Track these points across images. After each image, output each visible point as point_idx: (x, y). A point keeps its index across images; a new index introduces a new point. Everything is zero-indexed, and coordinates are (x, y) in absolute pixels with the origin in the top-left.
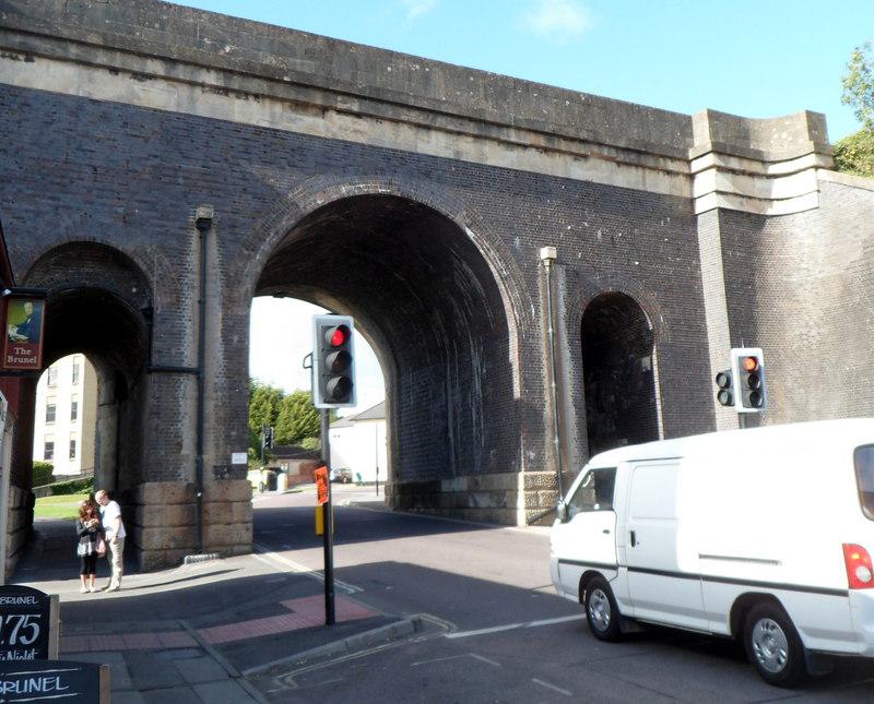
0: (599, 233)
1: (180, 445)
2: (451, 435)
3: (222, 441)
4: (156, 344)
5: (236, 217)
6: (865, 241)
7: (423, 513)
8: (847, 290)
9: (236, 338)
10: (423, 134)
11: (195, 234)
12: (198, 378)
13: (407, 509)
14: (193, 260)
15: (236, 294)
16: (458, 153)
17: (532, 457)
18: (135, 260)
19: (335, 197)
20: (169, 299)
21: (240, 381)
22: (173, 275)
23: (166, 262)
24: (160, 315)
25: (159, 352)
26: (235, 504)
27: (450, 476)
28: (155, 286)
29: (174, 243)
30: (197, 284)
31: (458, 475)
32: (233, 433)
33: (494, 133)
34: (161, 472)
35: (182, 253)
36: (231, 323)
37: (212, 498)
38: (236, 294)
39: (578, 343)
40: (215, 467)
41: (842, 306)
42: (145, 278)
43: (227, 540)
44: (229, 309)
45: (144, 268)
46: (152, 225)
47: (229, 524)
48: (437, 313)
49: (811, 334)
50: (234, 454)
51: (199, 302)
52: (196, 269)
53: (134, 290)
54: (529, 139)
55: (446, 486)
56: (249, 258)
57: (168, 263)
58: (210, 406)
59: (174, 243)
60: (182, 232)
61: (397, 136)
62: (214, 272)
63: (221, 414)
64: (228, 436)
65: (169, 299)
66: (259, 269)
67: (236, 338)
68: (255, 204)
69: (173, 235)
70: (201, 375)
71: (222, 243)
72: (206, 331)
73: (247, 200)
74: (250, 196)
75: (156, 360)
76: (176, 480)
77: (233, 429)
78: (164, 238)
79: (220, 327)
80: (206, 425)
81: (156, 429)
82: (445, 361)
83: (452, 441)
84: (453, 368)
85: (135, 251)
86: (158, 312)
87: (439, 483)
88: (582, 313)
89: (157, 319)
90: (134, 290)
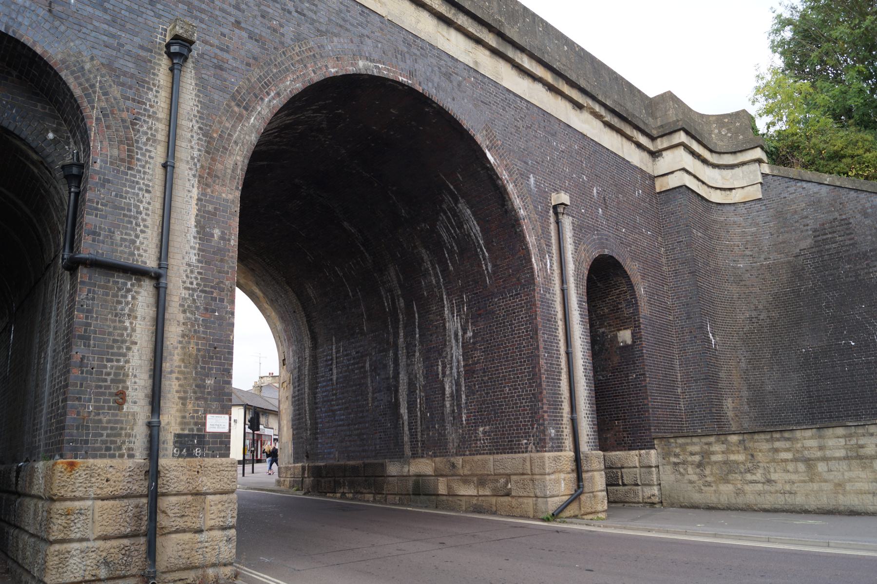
0: (595, 191)
1: (121, 397)
2: (404, 411)
3: (190, 394)
4: (89, 220)
5: (225, 55)
6: (815, 231)
7: (352, 499)
8: (797, 273)
9: (217, 232)
10: (443, 29)
11: (164, 63)
12: (157, 288)
13: (323, 493)
14: (160, 101)
15: (219, 166)
16: (476, 63)
17: (553, 435)
18: (63, 74)
19: (351, 70)
20: (115, 152)
21: (222, 300)
22: (125, 115)
23: (116, 91)
24: (97, 173)
25: (94, 233)
26: (210, 497)
27: (398, 455)
28: (93, 126)
29: (131, 67)
30: (161, 136)
31: (415, 456)
32: (208, 382)
33: (510, 53)
34: (86, 442)
35: (143, 83)
36: (210, 208)
37: (172, 488)
38: (219, 166)
39: (585, 305)
40: (178, 436)
41: (793, 291)
42: (76, 108)
43: (198, 559)
44: (208, 185)
45: (77, 92)
46: (96, 29)
47: (200, 531)
48: (392, 273)
49: (761, 317)
50: (209, 416)
51: (165, 166)
52: (162, 115)
53: (51, 136)
54: (539, 71)
55: (393, 469)
56: (240, 118)
57: (119, 96)
58: (173, 332)
59: (131, 67)
60: (143, 54)
61: (418, 22)
62: (188, 126)
63: (192, 349)
64: (201, 387)
65: (115, 152)
66: (254, 138)
67: (217, 232)
68: (252, 47)
69: (128, 53)
70: (162, 280)
71: (202, 85)
72: (174, 215)
73: (240, 38)
74: (245, 35)
75: (87, 248)
76: (113, 456)
77: (207, 376)
78: (114, 53)
79: (194, 211)
80: (166, 366)
81: (82, 364)
82: (396, 328)
83: (406, 417)
84: (410, 334)
85: (63, 61)
86: (97, 167)
87: (383, 466)
88: (586, 272)
89: (93, 180)
90: (51, 136)
